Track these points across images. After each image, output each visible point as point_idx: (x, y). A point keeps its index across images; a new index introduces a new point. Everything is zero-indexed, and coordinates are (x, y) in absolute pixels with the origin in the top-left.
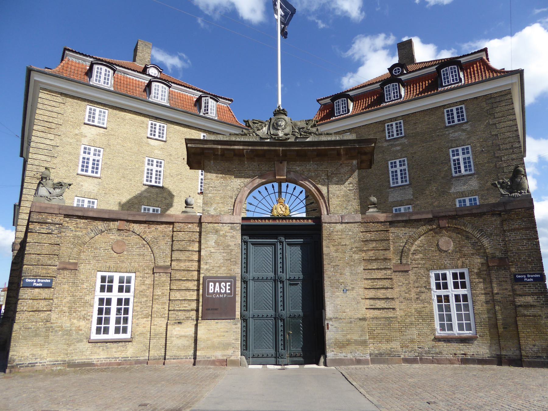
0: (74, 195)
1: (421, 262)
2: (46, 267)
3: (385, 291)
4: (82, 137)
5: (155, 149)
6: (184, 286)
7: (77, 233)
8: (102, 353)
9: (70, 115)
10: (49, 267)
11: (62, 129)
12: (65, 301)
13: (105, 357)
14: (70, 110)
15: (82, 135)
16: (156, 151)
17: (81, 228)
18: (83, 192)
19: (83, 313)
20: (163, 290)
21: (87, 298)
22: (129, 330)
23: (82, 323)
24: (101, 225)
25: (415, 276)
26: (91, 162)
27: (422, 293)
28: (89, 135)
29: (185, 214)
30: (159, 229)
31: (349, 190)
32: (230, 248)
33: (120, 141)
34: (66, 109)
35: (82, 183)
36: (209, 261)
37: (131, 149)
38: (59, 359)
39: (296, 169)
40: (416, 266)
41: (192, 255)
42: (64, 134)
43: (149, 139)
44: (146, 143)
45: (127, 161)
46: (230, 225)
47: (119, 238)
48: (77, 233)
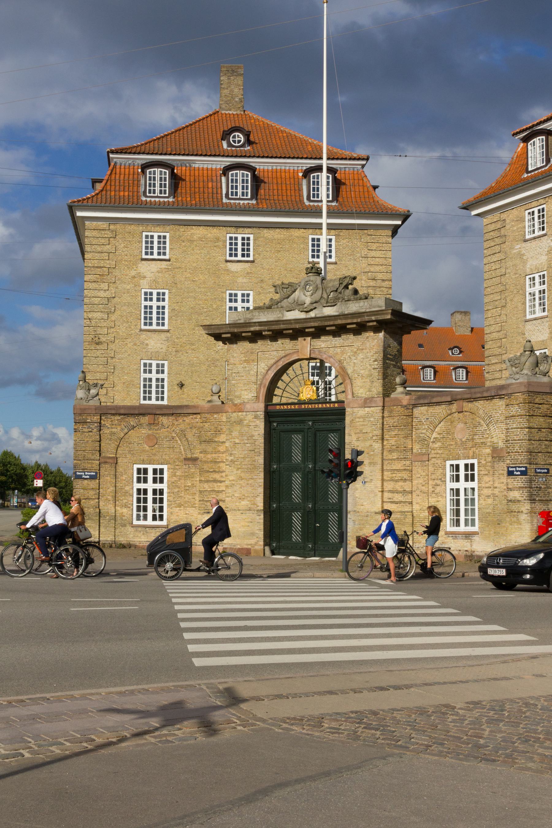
0: (139, 358)
1: (439, 452)
2: (91, 461)
3: (403, 484)
4: (140, 279)
5: (238, 277)
6: (212, 478)
7: (113, 430)
8: (143, 537)
9: (123, 251)
10: (93, 461)
11: (117, 273)
12: (109, 490)
13: (146, 540)
14: (122, 245)
15: (140, 276)
16: (240, 280)
17: (116, 425)
18: (149, 354)
19: (125, 501)
20: (192, 481)
21: (127, 488)
22: (165, 517)
23: (125, 510)
24: (132, 421)
25: (433, 466)
26: (155, 310)
27: (438, 485)
28: (148, 274)
29: (210, 404)
30: (187, 421)
31: (374, 369)
32: (254, 438)
33: (189, 275)
34: (117, 244)
35: (146, 342)
36: (234, 452)
37: (204, 283)
38: (108, 539)
39: (320, 346)
40: (435, 455)
41: (218, 446)
42: (119, 279)
43: (229, 264)
44: (225, 270)
45: (200, 302)
46: (254, 413)
47: (150, 432)
48: (113, 430)
